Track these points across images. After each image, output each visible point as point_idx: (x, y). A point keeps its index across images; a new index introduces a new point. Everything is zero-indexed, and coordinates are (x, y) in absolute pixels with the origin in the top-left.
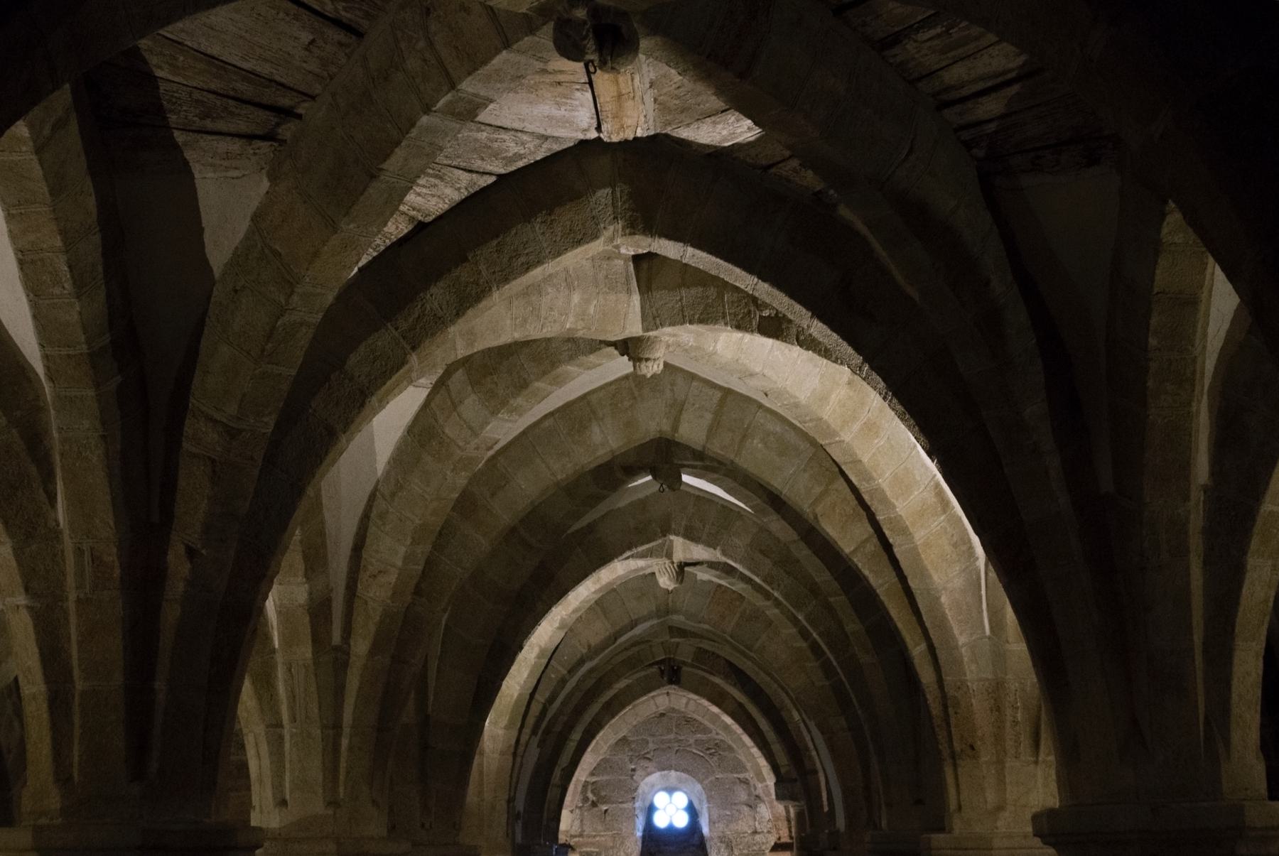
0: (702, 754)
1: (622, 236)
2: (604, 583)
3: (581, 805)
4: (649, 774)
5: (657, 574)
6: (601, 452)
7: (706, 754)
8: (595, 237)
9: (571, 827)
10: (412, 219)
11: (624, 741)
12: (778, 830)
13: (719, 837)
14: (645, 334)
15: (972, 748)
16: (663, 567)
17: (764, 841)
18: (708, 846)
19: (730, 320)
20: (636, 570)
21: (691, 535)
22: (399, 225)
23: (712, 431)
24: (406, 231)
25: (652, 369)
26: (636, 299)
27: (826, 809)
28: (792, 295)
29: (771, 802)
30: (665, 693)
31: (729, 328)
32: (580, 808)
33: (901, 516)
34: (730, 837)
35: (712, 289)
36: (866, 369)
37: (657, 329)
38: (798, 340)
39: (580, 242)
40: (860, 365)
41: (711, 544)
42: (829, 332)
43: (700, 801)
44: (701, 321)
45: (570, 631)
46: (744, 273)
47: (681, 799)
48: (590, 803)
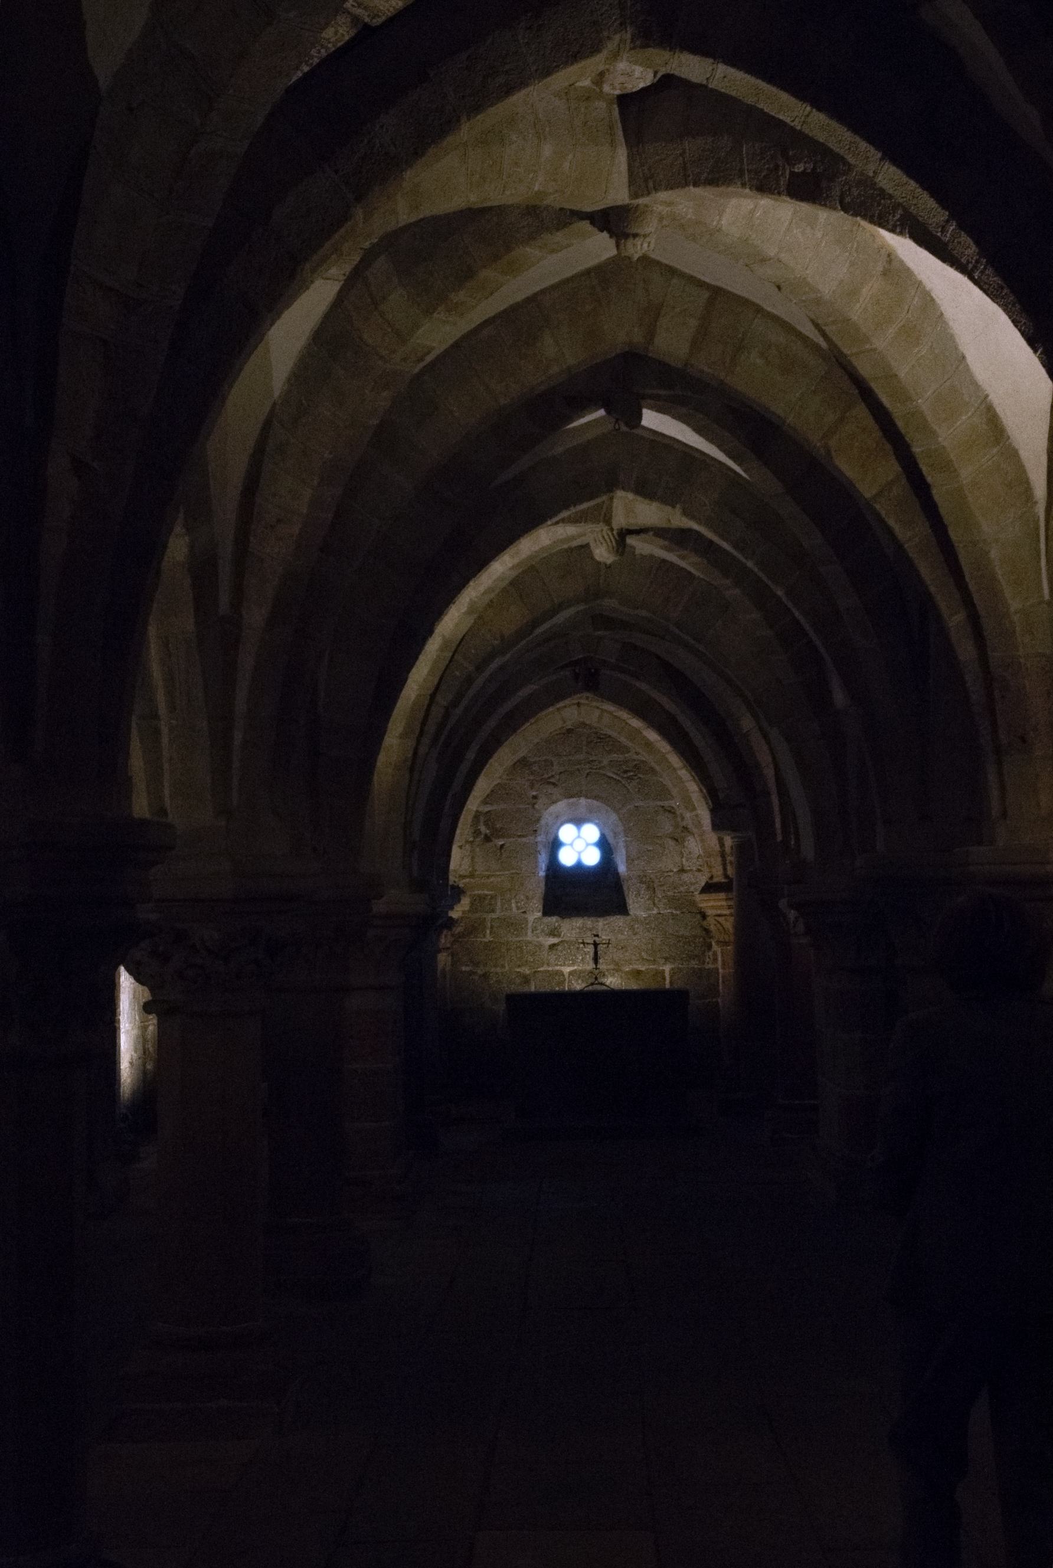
0: (618, 778)
1: (631, 49)
2: (524, 556)
3: (471, 839)
4: (554, 802)
5: (592, 545)
6: (555, 369)
7: (623, 778)
8: (595, 50)
9: (460, 865)
10: (355, 20)
11: (523, 763)
12: (710, 867)
13: (639, 876)
14: (633, 201)
15: (1023, 740)
16: (600, 536)
17: (693, 881)
18: (625, 888)
19: (749, 181)
20: (562, 541)
21: (644, 490)
22: (339, 28)
23: (695, 345)
24: (347, 38)
25: (637, 249)
26: (622, 155)
27: (779, 838)
28: (855, 128)
29: (702, 835)
30: (574, 704)
31: (747, 191)
32: (472, 842)
33: (944, 447)
34: (652, 876)
35: (726, 138)
36: (952, 228)
37: (649, 194)
38: (841, 202)
39: (575, 56)
40: (942, 223)
41: (668, 499)
42: (905, 178)
43: (615, 834)
44: (712, 182)
45: (481, 616)
46: (793, 100)
47: (591, 832)
48: (482, 836)
